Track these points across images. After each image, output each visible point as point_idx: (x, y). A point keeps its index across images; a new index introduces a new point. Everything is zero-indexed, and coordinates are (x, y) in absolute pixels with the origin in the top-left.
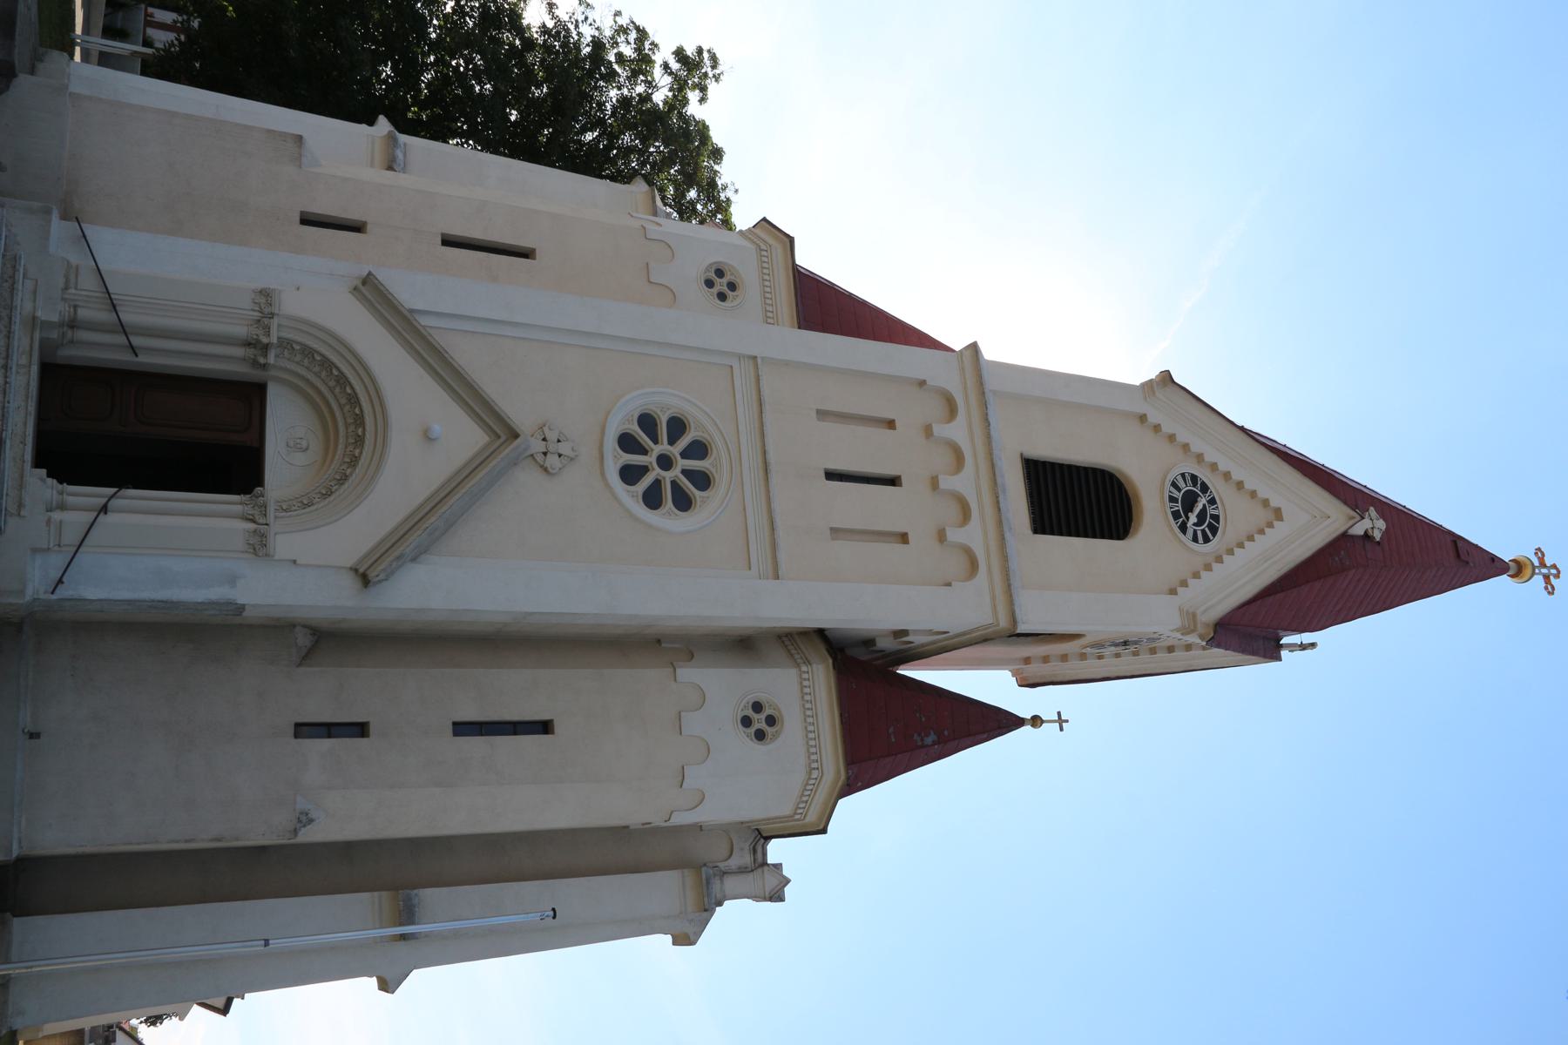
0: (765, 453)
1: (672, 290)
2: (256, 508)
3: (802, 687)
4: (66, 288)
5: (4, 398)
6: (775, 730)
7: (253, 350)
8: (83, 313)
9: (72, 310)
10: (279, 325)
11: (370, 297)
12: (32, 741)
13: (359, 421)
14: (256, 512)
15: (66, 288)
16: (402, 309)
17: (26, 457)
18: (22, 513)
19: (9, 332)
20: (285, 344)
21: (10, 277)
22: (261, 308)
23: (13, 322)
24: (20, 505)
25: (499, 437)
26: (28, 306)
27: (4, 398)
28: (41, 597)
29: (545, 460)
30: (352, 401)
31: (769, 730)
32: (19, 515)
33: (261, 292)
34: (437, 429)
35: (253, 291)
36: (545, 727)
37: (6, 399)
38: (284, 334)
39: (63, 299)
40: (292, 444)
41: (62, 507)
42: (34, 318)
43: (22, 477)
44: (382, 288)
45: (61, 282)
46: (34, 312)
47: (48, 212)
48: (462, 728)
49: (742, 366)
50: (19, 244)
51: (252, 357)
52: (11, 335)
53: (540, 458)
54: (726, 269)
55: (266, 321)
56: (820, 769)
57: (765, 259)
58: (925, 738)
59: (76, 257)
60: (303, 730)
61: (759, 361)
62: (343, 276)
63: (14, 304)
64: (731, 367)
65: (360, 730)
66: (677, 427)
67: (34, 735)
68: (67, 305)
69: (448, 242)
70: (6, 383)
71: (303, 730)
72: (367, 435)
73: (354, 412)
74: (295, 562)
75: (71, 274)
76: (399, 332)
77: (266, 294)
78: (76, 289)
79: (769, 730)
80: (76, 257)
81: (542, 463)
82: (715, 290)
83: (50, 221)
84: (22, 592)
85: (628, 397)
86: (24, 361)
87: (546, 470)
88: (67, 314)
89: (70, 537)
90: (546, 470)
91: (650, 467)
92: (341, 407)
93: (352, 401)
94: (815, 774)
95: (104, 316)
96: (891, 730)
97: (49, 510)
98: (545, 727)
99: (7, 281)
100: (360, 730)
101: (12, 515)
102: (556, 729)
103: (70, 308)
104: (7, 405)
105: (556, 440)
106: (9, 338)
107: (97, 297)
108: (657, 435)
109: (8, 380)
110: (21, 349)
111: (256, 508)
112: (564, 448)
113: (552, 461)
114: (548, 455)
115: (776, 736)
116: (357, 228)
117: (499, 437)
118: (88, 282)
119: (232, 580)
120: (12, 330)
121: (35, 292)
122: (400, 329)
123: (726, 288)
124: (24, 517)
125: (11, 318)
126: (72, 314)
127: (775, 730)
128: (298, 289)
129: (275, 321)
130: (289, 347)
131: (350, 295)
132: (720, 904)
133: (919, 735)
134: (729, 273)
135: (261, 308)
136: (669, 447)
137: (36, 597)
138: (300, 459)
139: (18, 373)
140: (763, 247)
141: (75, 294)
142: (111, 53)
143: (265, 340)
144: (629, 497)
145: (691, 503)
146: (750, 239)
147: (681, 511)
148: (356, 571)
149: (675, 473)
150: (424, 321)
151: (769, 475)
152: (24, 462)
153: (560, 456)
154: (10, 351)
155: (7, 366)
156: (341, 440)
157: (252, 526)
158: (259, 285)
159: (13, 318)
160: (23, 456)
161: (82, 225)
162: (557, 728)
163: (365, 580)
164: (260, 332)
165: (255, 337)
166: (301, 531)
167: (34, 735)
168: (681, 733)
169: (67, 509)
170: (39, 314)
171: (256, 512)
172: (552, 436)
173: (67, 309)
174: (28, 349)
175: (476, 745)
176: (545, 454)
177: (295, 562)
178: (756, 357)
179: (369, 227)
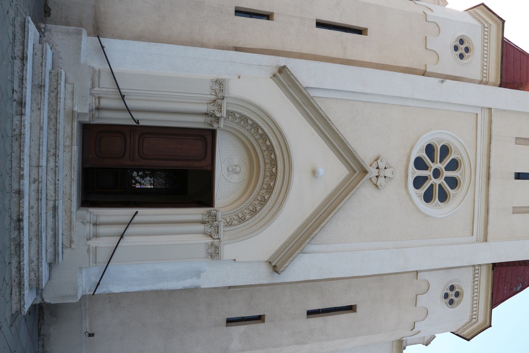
0: (489, 168)
1: (435, 51)
2: (212, 227)
3: (474, 277)
4: (93, 87)
5: (55, 177)
6: (458, 299)
7: (210, 118)
8: (104, 103)
9: (97, 100)
10: (227, 103)
11: (285, 83)
12: (90, 338)
13: (274, 163)
14: (212, 230)
15: (93, 87)
16: (300, 87)
17: (72, 209)
18: (72, 246)
19: (56, 129)
20: (230, 113)
21: (55, 89)
22: (216, 93)
23: (58, 122)
24: (71, 242)
25: (355, 172)
26: (69, 102)
27: (55, 177)
28: (87, 294)
29: (377, 181)
30: (270, 149)
31: (456, 299)
32: (71, 247)
33: (216, 81)
34: (321, 171)
35: (212, 81)
36: (351, 308)
37: (57, 178)
38: (230, 108)
39: (91, 94)
40: (230, 169)
41: (96, 236)
42: (73, 112)
43: (71, 222)
44: (292, 77)
45: (89, 84)
46: (73, 108)
47: (79, 33)
48: (311, 313)
49: (483, 113)
50: (61, 58)
51: (210, 122)
52: (58, 132)
53: (374, 180)
54: (465, 39)
55: (219, 101)
56: (477, 315)
57: (486, 33)
58: (518, 288)
59: (98, 64)
60: (231, 321)
61: (493, 110)
62: (267, 66)
63: (58, 109)
64: (477, 114)
65: (259, 318)
66: (445, 150)
67: (91, 335)
68: (94, 99)
69: (320, 24)
70: (56, 166)
71: (231, 321)
72: (279, 174)
73: (270, 156)
74: (235, 260)
75: (96, 74)
76: (301, 105)
77: (220, 83)
78: (99, 87)
79: (456, 299)
80: (98, 64)
81: (375, 183)
82: (458, 53)
83: (81, 40)
84: (76, 296)
85: (424, 137)
86: (68, 143)
87: (376, 186)
88: (94, 105)
89: (103, 257)
90: (376, 186)
91: (429, 177)
92: (265, 164)
93: (270, 149)
94: (474, 320)
95: (119, 104)
96: (505, 288)
97: (89, 239)
98: (351, 308)
99: (53, 92)
100: (259, 318)
101: (67, 247)
102: (358, 310)
103: (95, 100)
104: (57, 182)
105: (386, 176)
106: (56, 134)
107: (113, 92)
108: (434, 157)
109: (57, 164)
110: (65, 135)
111: (210, 217)
112: (388, 173)
113: (381, 180)
114: (379, 178)
115: (459, 302)
116: (268, 16)
117: (355, 172)
118: (106, 83)
119: (198, 274)
120: (58, 128)
121: (73, 93)
122: (302, 103)
123: (464, 51)
124: (74, 248)
125: (56, 119)
126: (97, 104)
127: (458, 299)
128: (239, 77)
129: (225, 101)
130: (232, 114)
131: (271, 80)
132: (405, 349)
133: (516, 287)
134: (466, 41)
135: (216, 93)
136: (444, 170)
137: (84, 294)
138: (236, 178)
139: (64, 151)
140: (486, 26)
141: (98, 91)
142: (67, 303)
143: (218, 115)
144: (416, 195)
145: (447, 197)
146: (476, 18)
147: (416, 169)
148: (270, 263)
149: (437, 165)
150: (313, 93)
151: (490, 181)
152: (71, 212)
153: (385, 177)
154: (57, 143)
155: (56, 154)
156: (262, 173)
157: (209, 240)
158: (215, 76)
159: (58, 120)
160: (71, 208)
161: (100, 38)
162: (358, 309)
163: (275, 269)
164: (215, 108)
165: (212, 112)
166: (239, 241)
167: (91, 335)
168: (416, 306)
169: (99, 237)
170: (76, 109)
171: (212, 230)
172: (382, 165)
173: (94, 101)
174: (70, 134)
175: (318, 321)
176: (377, 177)
177: (235, 260)
178: (491, 108)
179: (275, 16)
